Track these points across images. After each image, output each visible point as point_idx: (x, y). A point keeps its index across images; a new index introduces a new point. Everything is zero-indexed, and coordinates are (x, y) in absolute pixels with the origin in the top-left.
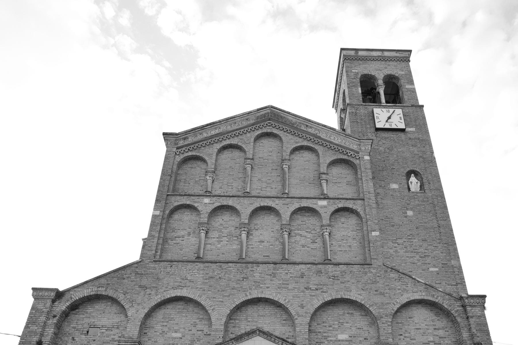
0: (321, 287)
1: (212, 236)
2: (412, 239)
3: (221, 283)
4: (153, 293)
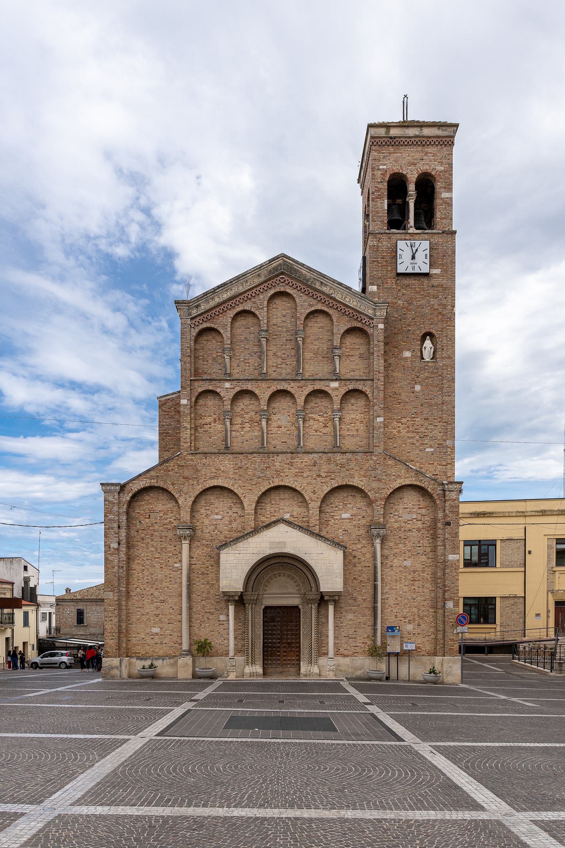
1: (235, 423)
2: (415, 418)
4: (195, 483)
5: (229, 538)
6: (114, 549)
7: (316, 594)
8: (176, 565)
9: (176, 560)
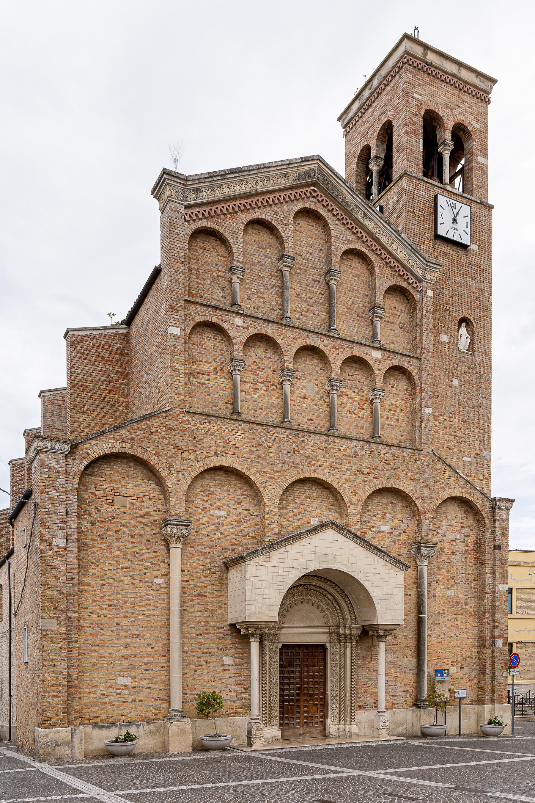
0: (373, 471)
3: (270, 454)
5: (236, 545)
6: (59, 547)
7: (357, 629)
8: (157, 581)
9: (157, 573)
